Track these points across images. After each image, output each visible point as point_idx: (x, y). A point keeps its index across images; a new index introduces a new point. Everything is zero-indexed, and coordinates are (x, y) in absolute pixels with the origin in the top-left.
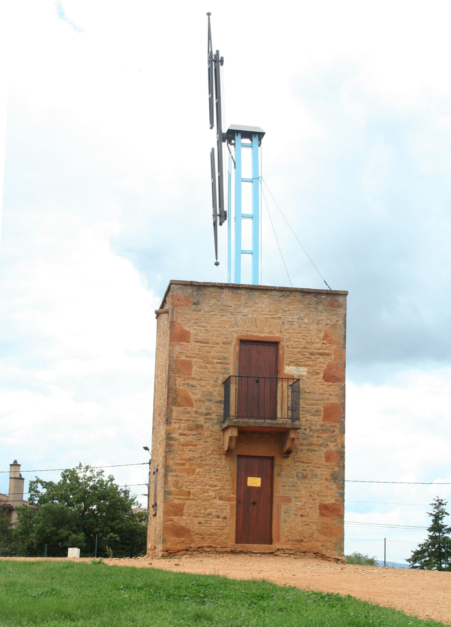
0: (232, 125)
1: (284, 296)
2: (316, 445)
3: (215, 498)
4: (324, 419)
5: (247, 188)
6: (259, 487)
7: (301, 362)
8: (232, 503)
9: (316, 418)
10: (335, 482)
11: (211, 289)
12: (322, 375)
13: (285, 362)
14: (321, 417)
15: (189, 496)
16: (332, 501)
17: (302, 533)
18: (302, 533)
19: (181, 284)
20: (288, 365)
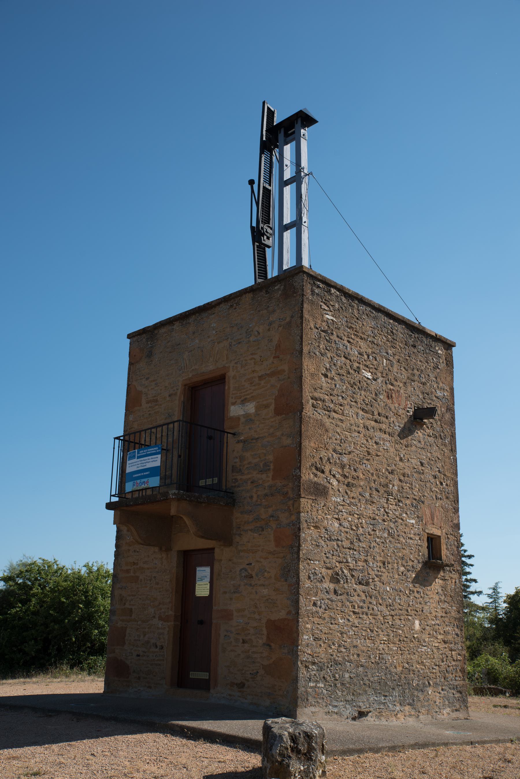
0: (305, 109)
1: (232, 306)
2: (512, 708)
3: (154, 617)
4: (274, 478)
5: (288, 191)
6: (114, 513)
7: (248, 395)
8: (169, 624)
9: (264, 476)
10: (286, 581)
11: (163, 330)
12: (272, 407)
13: (231, 400)
14: (270, 474)
15: (131, 616)
16: (283, 615)
17: (243, 672)
18: (243, 672)
19: (137, 335)
20: (234, 404)
